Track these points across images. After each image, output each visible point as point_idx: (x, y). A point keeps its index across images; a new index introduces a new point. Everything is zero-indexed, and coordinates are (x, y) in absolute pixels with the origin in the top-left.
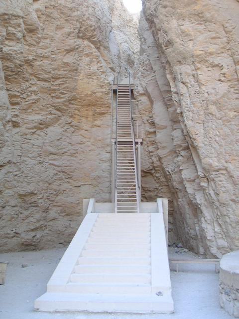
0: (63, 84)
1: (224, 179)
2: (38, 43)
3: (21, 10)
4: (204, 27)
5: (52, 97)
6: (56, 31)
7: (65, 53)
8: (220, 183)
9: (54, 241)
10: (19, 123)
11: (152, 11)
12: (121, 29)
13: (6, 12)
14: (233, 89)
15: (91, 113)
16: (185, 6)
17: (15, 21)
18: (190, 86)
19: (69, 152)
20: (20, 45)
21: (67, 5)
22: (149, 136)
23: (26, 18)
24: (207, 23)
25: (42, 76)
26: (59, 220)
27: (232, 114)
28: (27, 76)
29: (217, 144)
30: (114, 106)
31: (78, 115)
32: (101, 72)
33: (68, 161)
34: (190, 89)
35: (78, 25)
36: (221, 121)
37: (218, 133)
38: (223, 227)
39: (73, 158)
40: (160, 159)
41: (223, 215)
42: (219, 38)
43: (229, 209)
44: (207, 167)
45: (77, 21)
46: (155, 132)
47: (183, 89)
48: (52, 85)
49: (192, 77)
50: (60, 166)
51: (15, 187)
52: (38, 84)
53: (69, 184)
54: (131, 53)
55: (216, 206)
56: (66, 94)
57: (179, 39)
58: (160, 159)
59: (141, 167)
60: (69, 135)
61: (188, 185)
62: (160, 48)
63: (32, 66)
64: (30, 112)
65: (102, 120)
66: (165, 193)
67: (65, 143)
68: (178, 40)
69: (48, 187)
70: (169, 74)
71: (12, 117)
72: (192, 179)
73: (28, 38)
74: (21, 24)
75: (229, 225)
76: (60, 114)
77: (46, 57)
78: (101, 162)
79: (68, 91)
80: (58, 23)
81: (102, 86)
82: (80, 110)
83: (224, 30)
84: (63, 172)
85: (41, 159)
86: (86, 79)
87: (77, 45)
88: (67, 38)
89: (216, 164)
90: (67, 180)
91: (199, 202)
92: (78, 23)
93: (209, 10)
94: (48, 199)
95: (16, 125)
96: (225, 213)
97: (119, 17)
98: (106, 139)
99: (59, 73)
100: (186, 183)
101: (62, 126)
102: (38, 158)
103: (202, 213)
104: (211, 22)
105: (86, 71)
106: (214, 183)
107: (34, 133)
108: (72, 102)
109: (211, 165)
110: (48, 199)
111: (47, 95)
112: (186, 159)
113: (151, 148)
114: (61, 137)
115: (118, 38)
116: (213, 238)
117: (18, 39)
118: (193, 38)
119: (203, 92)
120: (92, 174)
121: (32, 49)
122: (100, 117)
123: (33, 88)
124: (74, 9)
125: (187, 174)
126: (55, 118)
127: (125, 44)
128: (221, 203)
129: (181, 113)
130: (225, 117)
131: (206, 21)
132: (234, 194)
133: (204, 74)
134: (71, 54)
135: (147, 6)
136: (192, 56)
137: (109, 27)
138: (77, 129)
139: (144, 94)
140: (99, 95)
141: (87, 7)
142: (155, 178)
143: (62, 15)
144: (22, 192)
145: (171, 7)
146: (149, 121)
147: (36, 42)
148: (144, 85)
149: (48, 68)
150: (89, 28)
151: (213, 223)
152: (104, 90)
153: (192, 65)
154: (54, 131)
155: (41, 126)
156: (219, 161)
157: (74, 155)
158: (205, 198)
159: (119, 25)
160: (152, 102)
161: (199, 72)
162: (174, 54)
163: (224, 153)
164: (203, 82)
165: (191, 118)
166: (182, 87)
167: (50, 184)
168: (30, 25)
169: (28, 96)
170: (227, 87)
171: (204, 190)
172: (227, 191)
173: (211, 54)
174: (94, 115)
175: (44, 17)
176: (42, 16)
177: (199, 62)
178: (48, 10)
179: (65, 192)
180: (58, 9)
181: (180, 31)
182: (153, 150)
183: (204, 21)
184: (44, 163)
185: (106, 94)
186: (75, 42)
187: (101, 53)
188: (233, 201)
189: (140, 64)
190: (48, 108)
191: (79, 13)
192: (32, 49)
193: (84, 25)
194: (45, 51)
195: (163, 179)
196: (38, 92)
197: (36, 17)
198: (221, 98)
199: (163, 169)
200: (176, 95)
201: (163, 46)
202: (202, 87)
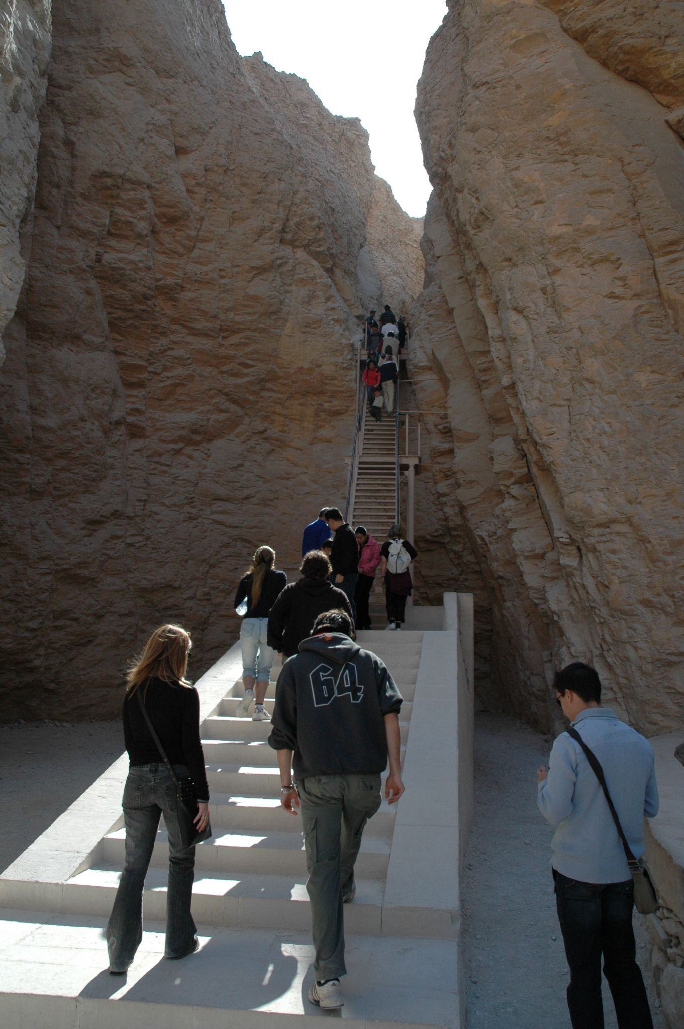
2: (191, 249)
3: (145, 168)
4: (572, 167)
5: (222, 373)
7: (251, 275)
8: (613, 557)
10: (143, 428)
11: (443, 151)
13: (107, 169)
17: (132, 193)
18: (536, 317)
20: (145, 251)
22: (439, 460)
23: (158, 190)
25: (198, 326)
28: (164, 323)
32: (333, 319)
35: (282, 214)
36: (614, 396)
37: (607, 429)
39: (267, 510)
43: (636, 625)
46: (451, 452)
47: (517, 325)
48: (221, 345)
49: (540, 293)
51: (131, 572)
52: (188, 343)
55: (599, 616)
56: (252, 366)
57: (509, 204)
58: (462, 509)
59: (416, 530)
61: (527, 567)
63: (173, 299)
64: (170, 405)
68: (506, 207)
69: (208, 572)
71: (127, 414)
72: (538, 551)
73: (166, 238)
74: (146, 202)
76: (240, 412)
79: (257, 360)
84: (244, 540)
85: (194, 511)
87: (277, 259)
89: (601, 506)
91: (554, 607)
92: (281, 209)
94: (207, 600)
95: (136, 432)
96: (625, 636)
97: (382, 221)
102: (187, 508)
103: (562, 634)
107: (178, 452)
108: (269, 385)
110: (207, 600)
111: (209, 369)
112: (524, 506)
113: (442, 487)
114: (240, 461)
117: (139, 236)
118: (544, 196)
121: (175, 262)
123: (180, 352)
125: (526, 539)
127: (395, 278)
129: (513, 386)
132: (650, 586)
139: (430, 369)
140: (328, 370)
142: (452, 555)
144: (145, 582)
146: (440, 427)
147: (184, 246)
150: (309, 223)
152: (340, 359)
154: (224, 448)
155: (197, 438)
158: (571, 597)
159: (381, 238)
160: (445, 382)
161: (558, 279)
167: (212, 566)
168: (167, 206)
169: (166, 369)
171: (570, 575)
174: (317, 415)
175: (203, 191)
176: (196, 189)
177: (560, 254)
181: (509, 184)
183: (573, 151)
184: (200, 519)
185: (344, 368)
187: (333, 281)
188: (647, 603)
190: (212, 397)
192: (175, 262)
194: (205, 269)
195: (469, 558)
196: (189, 361)
197: (183, 188)
200: (499, 345)
201: (468, 228)
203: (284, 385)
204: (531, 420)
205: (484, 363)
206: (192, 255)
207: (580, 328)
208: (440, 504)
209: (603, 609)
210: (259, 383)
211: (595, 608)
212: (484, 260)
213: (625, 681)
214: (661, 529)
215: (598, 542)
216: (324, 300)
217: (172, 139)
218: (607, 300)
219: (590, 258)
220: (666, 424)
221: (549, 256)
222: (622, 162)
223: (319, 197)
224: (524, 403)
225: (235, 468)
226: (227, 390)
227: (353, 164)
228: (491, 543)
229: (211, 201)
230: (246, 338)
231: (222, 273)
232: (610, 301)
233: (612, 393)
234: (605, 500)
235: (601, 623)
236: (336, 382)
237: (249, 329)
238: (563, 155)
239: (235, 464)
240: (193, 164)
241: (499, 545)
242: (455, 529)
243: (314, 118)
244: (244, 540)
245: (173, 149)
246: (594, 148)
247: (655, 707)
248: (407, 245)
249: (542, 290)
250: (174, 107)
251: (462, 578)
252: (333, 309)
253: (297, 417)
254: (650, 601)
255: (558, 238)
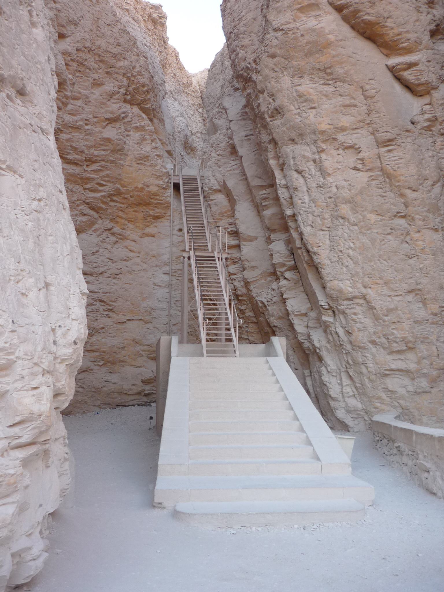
0: (101, 170)
1: (360, 312)
4: (334, 89)
5: (85, 189)
6: (92, 88)
7: (105, 124)
8: (354, 316)
9: (86, 403)
11: (249, 64)
12: (176, 97)
14: (374, 182)
15: (140, 215)
16: (305, 55)
18: (310, 177)
19: (109, 271)
21: (109, 50)
24: (338, 83)
25: (71, 157)
26: (94, 371)
27: (373, 218)
29: (350, 260)
30: (174, 206)
31: (121, 218)
32: (156, 155)
33: (108, 285)
34: (308, 180)
35: (126, 83)
36: (356, 228)
37: (352, 245)
38: (356, 380)
39: (114, 281)
40: (247, 284)
41: (356, 363)
42: (355, 106)
43: (367, 355)
44: (334, 293)
45: (124, 75)
46: (238, 246)
47: (298, 180)
49: (312, 163)
50: (96, 292)
53: (109, 320)
54: (189, 134)
57: (294, 106)
58: (247, 284)
60: (109, 246)
62: (254, 116)
65: (156, 227)
66: (252, 333)
67: (103, 258)
68: (292, 108)
70: (272, 158)
75: (365, 378)
76: (96, 216)
77: (78, 128)
78: (156, 287)
79: (108, 181)
80: (96, 76)
81: (158, 177)
82: (126, 211)
83: (363, 94)
84: (101, 301)
86: (136, 165)
87: (123, 113)
88: (109, 100)
90: (107, 313)
92: (125, 79)
93: (342, 63)
96: (361, 360)
97: (173, 77)
98: (163, 254)
99: (96, 153)
100: (294, 318)
101: (98, 232)
103: (320, 359)
104: (344, 81)
105: (135, 152)
106: (345, 317)
108: (115, 198)
109: (340, 291)
111: (78, 186)
112: (293, 284)
114: (97, 249)
115: (172, 109)
116: (340, 397)
118: (316, 105)
119: (330, 185)
120: (143, 305)
122: (154, 223)
124: (119, 56)
126: (89, 220)
127: (181, 119)
128: (354, 346)
129: (294, 215)
130: (363, 221)
131: (336, 80)
133: (331, 159)
134: (114, 126)
135: (240, 55)
136: (314, 133)
137: (162, 92)
138: (121, 239)
139: (220, 191)
141: (138, 55)
143: (101, 64)
145: (283, 57)
146: (229, 230)
147: (63, 103)
148: (219, 177)
149: (81, 145)
150: (142, 88)
151: (340, 374)
152: (161, 182)
153: (313, 146)
156: (353, 286)
157: (117, 277)
159: (172, 89)
160: (232, 202)
161: (324, 156)
162: (284, 129)
163: (361, 274)
164: (330, 170)
165: (310, 222)
166: (296, 179)
170: (366, 179)
172: (365, 328)
173: (343, 129)
175: (75, 64)
176: (71, 63)
177: (325, 141)
178: (81, 55)
179: (103, 330)
180: (95, 54)
181: (295, 95)
182: (235, 272)
183: (333, 79)
186: (120, 108)
188: (373, 342)
189: (212, 147)
190: (78, 206)
191: (126, 62)
193: (133, 83)
194: (76, 118)
195: (249, 314)
197: (63, 63)
198: (357, 194)
199: (251, 299)
200: (284, 190)
201: (266, 116)
202: (328, 178)
203: (125, 198)
204: (307, 238)
205: (264, 194)
206: (67, 109)
207: (336, 186)
208: (231, 279)
209: (347, 346)
210: (109, 197)
211: (343, 345)
212: (276, 137)
213: (360, 386)
214: (382, 302)
215: (346, 309)
216: (150, 142)
217: (57, 28)
218: (352, 171)
219: (343, 145)
220: (384, 244)
221: (318, 142)
222: (362, 89)
223: (147, 70)
224: (302, 227)
225: (93, 254)
226: (88, 201)
227: (156, 37)
228: (269, 306)
229: (80, 71)
230: (102, 166)
231: (87, 122)
232: (354, 172)
233: (354, 225)
234: (350, 285)
235: (346, 353)
236: (158, 197)
237: (104, 161)
238: (328, 80)
239: (94, 250)
240: (69, 45)
241: (274, 307)
242: (241, 296)
243: (132, 3)
244: (101, 301)
245: (57, 35)
246: (346, 79)
247: (377, 399)
248: (188, 94)
249: (313, 161)
250: (58, 6)
251: (245, 326)
252: (156, 148)
253: (132, 220)
254: (375, 341)
255: (324, 131)
